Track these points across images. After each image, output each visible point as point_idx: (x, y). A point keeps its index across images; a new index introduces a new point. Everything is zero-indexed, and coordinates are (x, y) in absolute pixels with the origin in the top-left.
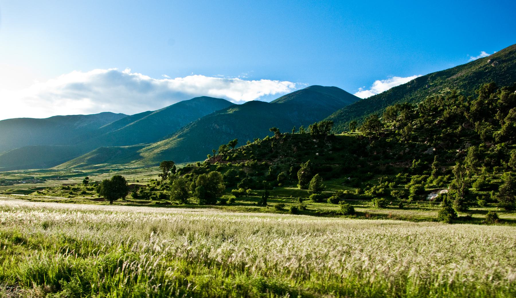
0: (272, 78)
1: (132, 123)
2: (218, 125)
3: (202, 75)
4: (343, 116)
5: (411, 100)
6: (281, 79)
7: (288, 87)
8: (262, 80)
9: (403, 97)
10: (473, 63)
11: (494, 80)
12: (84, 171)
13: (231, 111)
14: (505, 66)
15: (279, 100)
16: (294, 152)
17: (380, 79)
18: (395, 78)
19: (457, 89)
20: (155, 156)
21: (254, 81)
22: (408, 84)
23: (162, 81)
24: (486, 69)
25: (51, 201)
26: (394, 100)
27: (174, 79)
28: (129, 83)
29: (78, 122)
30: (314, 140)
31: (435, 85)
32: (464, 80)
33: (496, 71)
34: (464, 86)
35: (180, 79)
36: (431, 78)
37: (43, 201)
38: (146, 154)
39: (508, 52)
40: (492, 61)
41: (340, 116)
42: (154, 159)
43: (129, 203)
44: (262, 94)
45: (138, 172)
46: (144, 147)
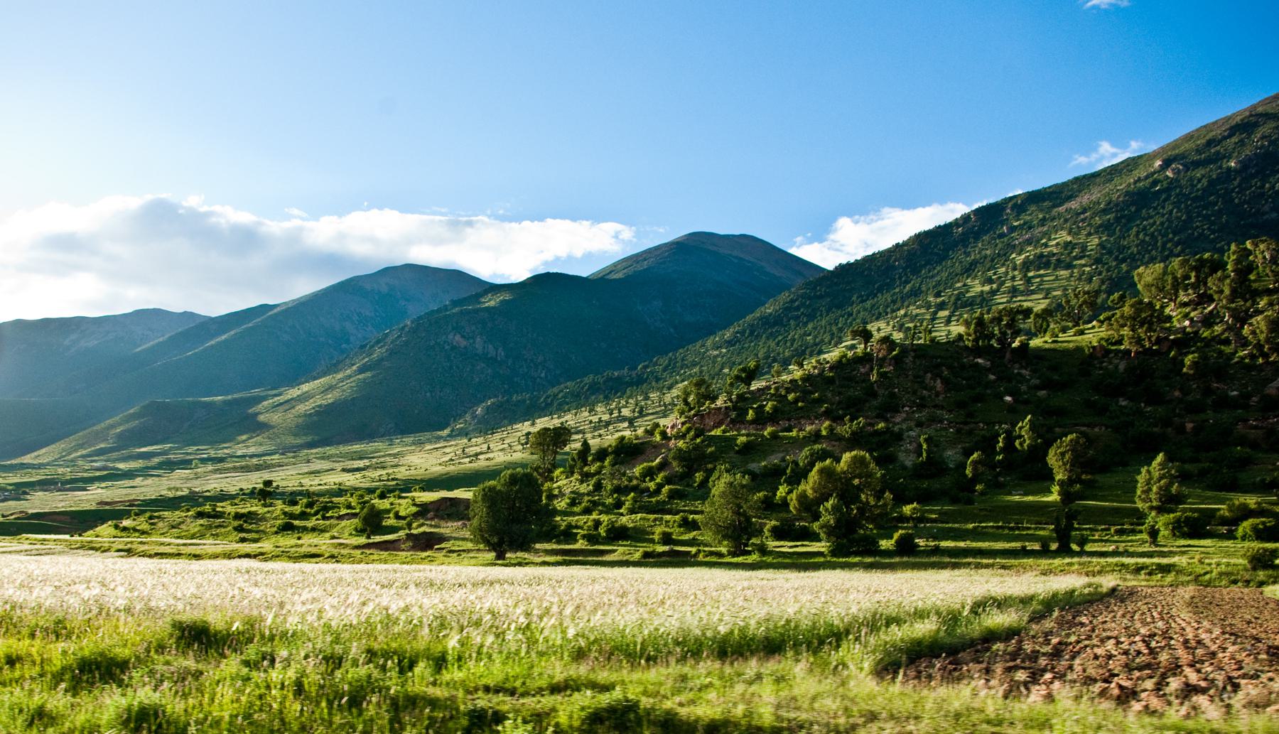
1: (223, 337)
2: (463, 337)
3: (392, 209)
4: (798, 308)
5: (971, 264)
6: (597, 216)
7: (616, 237)
8: (549, 220)
10: (1113, 171)
11: (1179, 210)
12: (121, 466)
13: (491, 302)
14: (1203, 176)
15: (614, 268)
16: (937, 395)
17: (850, 215)
18: (886, 210)
19: (1089, 234)
20: (300, 420)
21: (526, 223)
22: (956, 223)
23: (287, 225)
24: (1155, 183)
26: (924, 266)
27: (317, 220)
28: (198, 229)
29: (73, 337)
30: (980, 361)
31: (1029, 226)
32: (1104, 211)
33: (1181, 187)
34: (1106, 228)
35: (335, 218)
36: (1012, 209)
37: (197, 557)
38: (275, 418)
39: (1204, 141)
40: (1167, 163)
41: (788, 309)
42: (299, 430)
44: (549, 256)
45: (273, 466)
46: (265, 398)
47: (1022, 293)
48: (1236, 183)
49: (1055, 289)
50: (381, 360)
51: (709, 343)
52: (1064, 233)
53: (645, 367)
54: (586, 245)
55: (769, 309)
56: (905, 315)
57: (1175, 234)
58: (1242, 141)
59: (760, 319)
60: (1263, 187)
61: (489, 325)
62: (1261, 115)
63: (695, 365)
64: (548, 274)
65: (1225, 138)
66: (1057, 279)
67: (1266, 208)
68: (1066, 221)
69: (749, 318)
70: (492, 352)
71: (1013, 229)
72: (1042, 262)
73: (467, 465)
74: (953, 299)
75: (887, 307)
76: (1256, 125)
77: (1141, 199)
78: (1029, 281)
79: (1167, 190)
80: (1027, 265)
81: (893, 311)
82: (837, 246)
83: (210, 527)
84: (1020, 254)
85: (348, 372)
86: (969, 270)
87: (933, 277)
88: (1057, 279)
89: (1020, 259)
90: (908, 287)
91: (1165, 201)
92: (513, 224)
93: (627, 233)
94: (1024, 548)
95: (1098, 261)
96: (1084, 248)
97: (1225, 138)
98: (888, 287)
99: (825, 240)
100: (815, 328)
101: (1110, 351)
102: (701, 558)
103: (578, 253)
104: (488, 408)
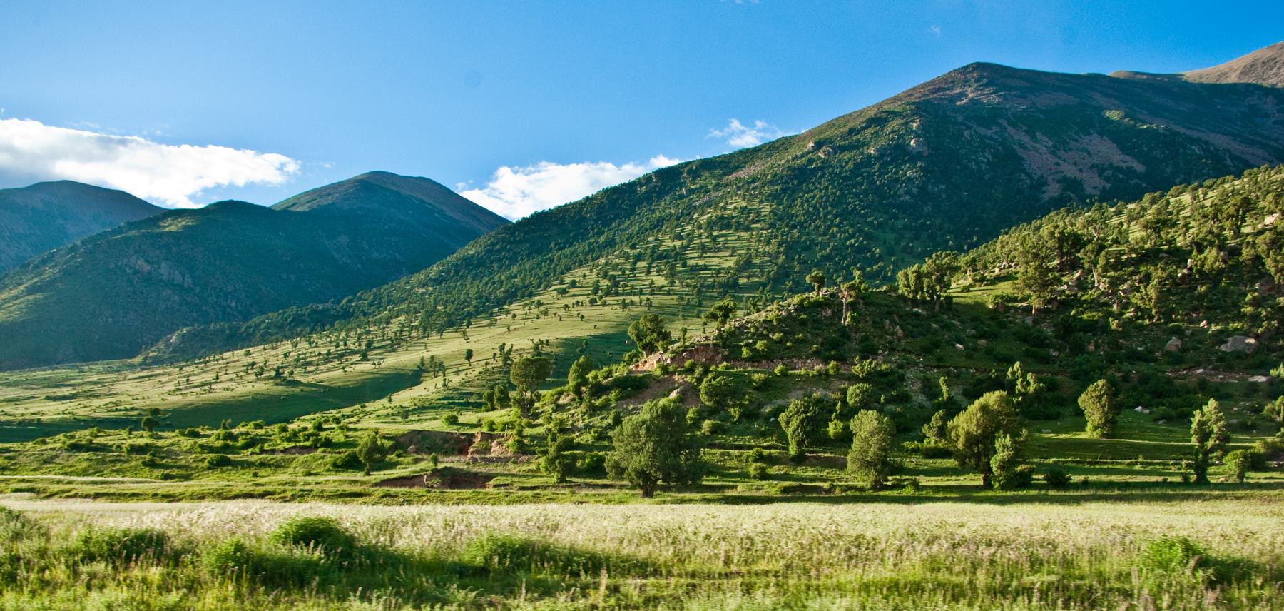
0: (238, 143)
2: (147, 261)
4: (499, 252)
8: (211, 147)
9: (632, 213)
13: (173, 227)
15: (296, 200)
17: (510, 166)
18: (544, 163)
19: (761, 202)
21: (185, 147)
24: (811, 161)
25: (97, 496)
26: (614, 220)
32: (771, 183)
34: (775, 197)
40: (819, 145)
43: (709, 495)
47: (710, 250)
48: (876, 167)
49: (738, 248)
50: (53, 281)
51: (414, 280)
52: (739, 199)
53: (350, 301)
54: (260, 175)
55: (471, 250)
56: (607, 264)
57: (833, 207)
58: (876, 132)
59: (464, 259)
60: (897, 173)
61: (174, 250)
62: (889, 112)
63: (403, 300)
64: (231, 202)
65: (863, 129)
66: (738, 239)
67: (901, 191)
68: (739, 188)
69: (451, 258)
70: (178, 277)
71: (691, 192)
72: (724, 223)
73: (195, 397)
74: (649, 251)
75: (587, 254)
76: (886, 120)
77: (801, 175)
78: (714, 239)
79: (821, 169)
80: (711, 225)
81: (593, 260)
82: (496, 193)
83: (104, 462)
84: (702, 214)
85: (14, 292)
86: (658, 225)
87: (623, 230)
88: (738, 239)
89: (704, 219)
90: (602, 238)
91: (821, 177)
92: (172, 147)
93: (292, 167)
94: (1165, 481)
95: (772, 226)
96: (759, 214)
97: (863, 129)
98: (582, 236)
99: (485, 187)
100: (519, 271)
101: (1009, 308)
102: (837, 492)
103: (241, 182)
104: (184, 336)
